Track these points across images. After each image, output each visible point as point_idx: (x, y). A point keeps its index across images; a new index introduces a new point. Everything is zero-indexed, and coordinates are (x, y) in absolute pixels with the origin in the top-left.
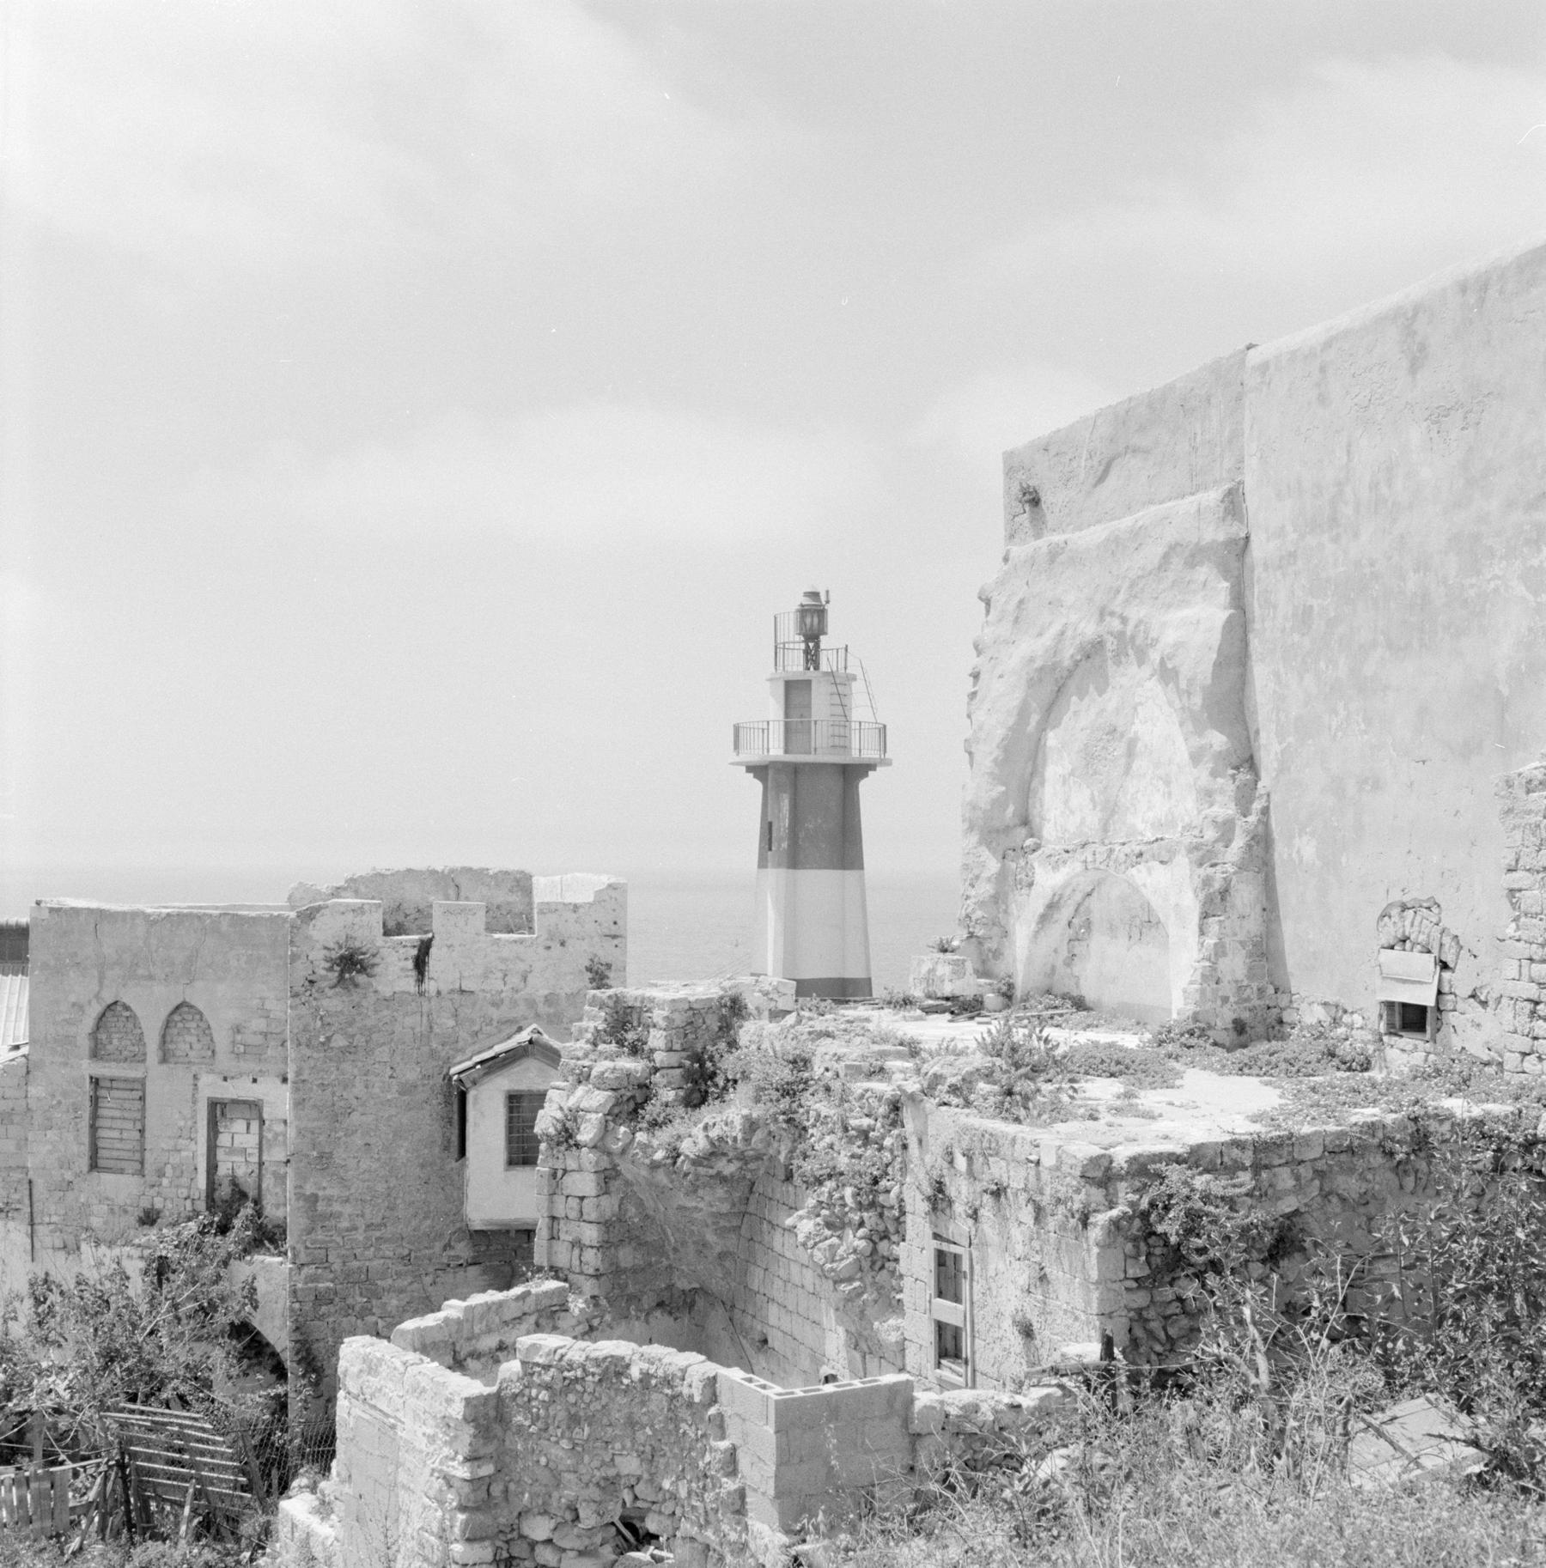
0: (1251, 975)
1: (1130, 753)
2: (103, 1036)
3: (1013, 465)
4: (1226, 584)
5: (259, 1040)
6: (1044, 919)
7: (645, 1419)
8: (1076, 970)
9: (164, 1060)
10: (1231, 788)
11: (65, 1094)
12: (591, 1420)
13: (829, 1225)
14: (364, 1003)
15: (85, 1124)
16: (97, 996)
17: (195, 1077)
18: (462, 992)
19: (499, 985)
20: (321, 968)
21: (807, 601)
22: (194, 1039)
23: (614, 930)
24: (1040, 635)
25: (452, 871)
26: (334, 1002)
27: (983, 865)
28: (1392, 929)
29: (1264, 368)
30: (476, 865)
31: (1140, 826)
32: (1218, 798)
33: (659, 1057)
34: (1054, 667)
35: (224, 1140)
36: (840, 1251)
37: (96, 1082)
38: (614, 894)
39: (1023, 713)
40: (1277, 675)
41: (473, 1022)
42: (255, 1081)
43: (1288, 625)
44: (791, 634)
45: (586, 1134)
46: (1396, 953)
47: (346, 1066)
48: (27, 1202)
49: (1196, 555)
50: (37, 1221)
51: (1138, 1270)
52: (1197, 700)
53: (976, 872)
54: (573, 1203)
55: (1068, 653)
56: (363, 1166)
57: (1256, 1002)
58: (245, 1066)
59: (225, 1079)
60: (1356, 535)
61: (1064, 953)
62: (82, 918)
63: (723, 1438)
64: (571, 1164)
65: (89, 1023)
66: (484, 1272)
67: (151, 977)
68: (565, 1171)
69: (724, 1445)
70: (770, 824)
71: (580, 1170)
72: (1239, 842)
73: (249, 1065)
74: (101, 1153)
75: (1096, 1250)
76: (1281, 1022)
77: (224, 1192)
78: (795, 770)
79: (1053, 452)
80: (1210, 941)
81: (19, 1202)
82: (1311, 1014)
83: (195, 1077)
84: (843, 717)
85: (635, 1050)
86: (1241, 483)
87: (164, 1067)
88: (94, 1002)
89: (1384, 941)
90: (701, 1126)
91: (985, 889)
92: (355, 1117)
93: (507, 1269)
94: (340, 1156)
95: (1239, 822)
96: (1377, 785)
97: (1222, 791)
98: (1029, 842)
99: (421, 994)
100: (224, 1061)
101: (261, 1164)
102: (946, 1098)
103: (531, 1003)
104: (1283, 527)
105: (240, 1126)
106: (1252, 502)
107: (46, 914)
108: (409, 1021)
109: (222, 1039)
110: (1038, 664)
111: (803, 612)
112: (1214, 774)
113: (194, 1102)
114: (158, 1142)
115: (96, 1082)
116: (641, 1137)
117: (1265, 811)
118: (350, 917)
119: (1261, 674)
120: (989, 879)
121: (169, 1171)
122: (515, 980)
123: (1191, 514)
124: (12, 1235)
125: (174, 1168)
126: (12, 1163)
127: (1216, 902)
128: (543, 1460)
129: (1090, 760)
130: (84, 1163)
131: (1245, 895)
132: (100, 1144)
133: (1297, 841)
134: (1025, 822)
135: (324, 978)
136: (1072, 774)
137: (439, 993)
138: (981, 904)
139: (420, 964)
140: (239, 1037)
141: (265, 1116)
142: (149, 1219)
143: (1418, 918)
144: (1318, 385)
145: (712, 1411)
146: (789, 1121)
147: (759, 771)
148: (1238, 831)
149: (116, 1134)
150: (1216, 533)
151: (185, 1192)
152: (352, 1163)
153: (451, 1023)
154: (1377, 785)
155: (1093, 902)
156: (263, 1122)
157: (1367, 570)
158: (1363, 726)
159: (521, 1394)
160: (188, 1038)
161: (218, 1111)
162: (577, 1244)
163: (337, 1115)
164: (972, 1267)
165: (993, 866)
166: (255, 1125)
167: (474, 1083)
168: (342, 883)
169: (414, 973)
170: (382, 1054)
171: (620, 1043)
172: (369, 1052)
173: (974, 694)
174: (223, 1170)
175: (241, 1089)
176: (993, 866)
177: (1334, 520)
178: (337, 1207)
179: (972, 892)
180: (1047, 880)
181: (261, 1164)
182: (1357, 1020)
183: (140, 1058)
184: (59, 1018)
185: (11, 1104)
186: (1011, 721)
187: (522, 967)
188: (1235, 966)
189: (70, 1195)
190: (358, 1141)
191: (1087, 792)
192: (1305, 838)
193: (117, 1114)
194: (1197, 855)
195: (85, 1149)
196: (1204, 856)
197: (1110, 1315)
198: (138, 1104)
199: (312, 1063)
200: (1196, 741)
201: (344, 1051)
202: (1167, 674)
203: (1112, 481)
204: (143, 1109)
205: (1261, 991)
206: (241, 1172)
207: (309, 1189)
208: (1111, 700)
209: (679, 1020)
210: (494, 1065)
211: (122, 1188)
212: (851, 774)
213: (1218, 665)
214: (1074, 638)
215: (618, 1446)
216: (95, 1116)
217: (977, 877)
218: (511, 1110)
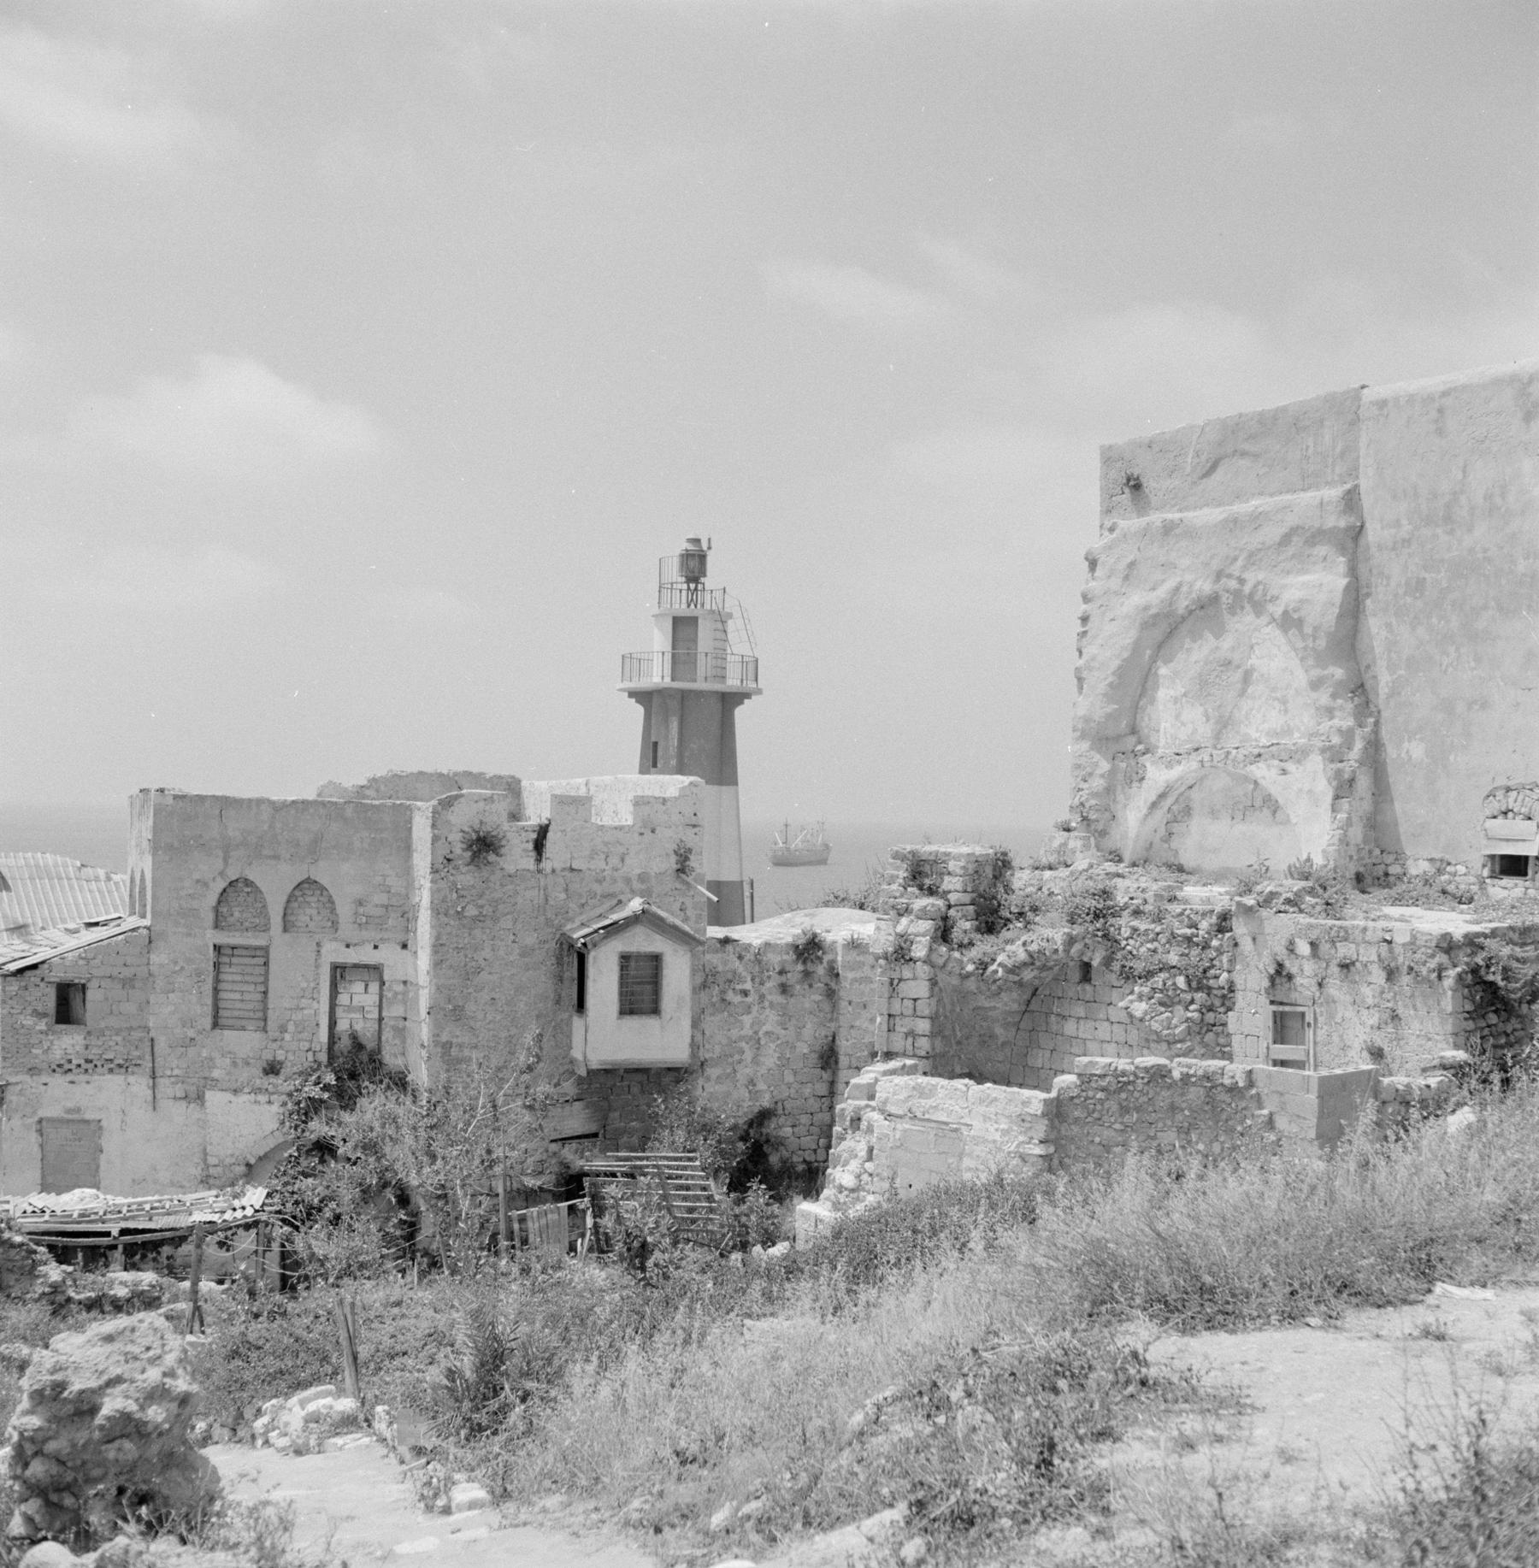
0: (1365, 842)
1: (1247, 678)
2: (224, 910)
3: (1109, 457)
4: (1342, 559)
5: (380, 912)
6: (1154, 805)
7: (1184, 1105)
8: (1174, 845)
9: (285, 930)
10: (1350, 706)
11: (189, 961)
12: (1138, 1109)
13: (1162, 1004)
14: (492, 878)
15: (208, 987)
16: (221, 874)
17: (318, 944)
18: (572, 870)
19: (602, 865)
20: (458, 849)
21: (691, 547)
22: (314, 912)
23: (694, 820)
24: (1154, 589)
25: (456, 774)
26: (467, 878)
27: (1096, 765)
28: (1496, 805)
29: (1382, 404)
30: (475, 770)
31: (1255, 735)
32: (1337, 713)
33: (953, 898)
34: (1168, 615)
35: (343, 999)
36: (1174, 1021)
37: (217, 948)
38: (694, 790)
39: (1137, 648)
40: (1389, 626)
41: (580, 896)
42: (376, 947)
43: (1401, 591)
44: (674, 574)
45: (919, 951)
46: (1500, 820)
47: (477, 932)
48: (148, 1057)
49: (1316, 537)
50: (159, 1073)
51: (1469, 1007)
52: (1322, 643)
53: (1089, 770)
54: (910, 1004)
55: (1182, 605)
56: (489, 1017)
57: (1368, 861)
58: (365, 934)
59: (348, 946)
60: (1470, 530)
61: (1162, 832)
62: (207, 804)
63: (1261, 1107)
64: (907, 974)
65: (212, 899)
66: (587, 1107)
67: (276, 857)
68: (900, 980)
69: (1265, 1112)
70: (655, 744)
71: (915, 978)
72: (1359, 745)
73: (371, 934)
74: (221, 1012)
75: (1450, 993)
76: (1387, 874)
77: (344, 1044)
78: (685, 698)
79: (1156, 448)
80: (1342, 816)
81: (139, 1058)
82: (1418, 867)
83: (318, 944)
84: (720, 656)
85: (931, 892)
86: (1357, 486)
87: (287, 936)
88: (219, 879)
89: (1488, 813)
90: (1020, 942)
91: (1098, 783)
92: (484, 975)
93: (605, 1104)
94: (471, 1008)
95: (1358, 731)
96: (1485, 705)
97: (1341, 708)
98: (1140, 747)
99: (539, 871)
100: (347, 930)
101: (381, 1019)
102: (1283, 908)
103: (628, 881)
104: (1398, 521)
105: (358, 987)
106: (1367, 502)
107: (170, 801)
108: (529, 894)
109: (344, 910)
110: (1153, 611)
111: (686, 557)
112: (1334, 696)
113: (317, 967)
114: (279, 1002)
115: (217, 948)
116: (956, 954)
117: (1377, 724)
118: (481, 804)
119: (1375, 626)
120: (1102, 776)
121: (291, 1027)
122: (614, 861)
123: (1317, 502)
124: (134, 1089)
125: (296, 1025)
126: (135, 1024)
127: (1344, 788)
128: (1097, 1140)
129: (1203, 687)
130: (207, 1022)
131: (1364, 783)
132: (222, 1004)
133: (1406, 744)
134: (1134, 731)
135: (460, 857)
136: (1185, 695)
137: (553, 871)
138: (1094, 795)
139: (539, 846)
140: (361, 910)
141: (386, 978)
142: (272, 1069)
143: (1521, 797)
144: (1436, 421)
145: (1254, 1091)
146: (1104, 936)
147: (643, 697)
148: (1357, 738)
149: (237, 996)
150: (1337, 521)
151: (307, 1045)
152: (480, 1015)
153: (563, 896)
154: (1485, 705)
155: (1195, 795)
156: (383, 983)
157: (1480, 556)
158: (1473, 664)
159: (1078, 1096)
160: (308, 911)
161: (339, 973)
162: (911, 1034)
163: (469, 974)
164: (1316, 1019)
165: (1105, 766)
166: (374, 987)
167: (595, 945)
168: (364, 782)
169: (533, 854)
170: (506, 923)
171: (921, 888)
172: (496, 920)
173: (1085, 633)
174: (343, 1026)
175: (366, 955)
176: (1105, 766)
177: (1448, 519)
178: (466, 1053)
179: (1085, 786)
180: (1158, 776)
181: (381, 1019)
182: (1461, 869)
183: (266, 928)
184: (183, 893)
185: (132, 970)
186: (1126, 655)
187: (621, 850)
188: (1357, 833)
189: (192, 1051)
190: (485, 996)
191: (1201, 709)
192: (1414, 743)
193: (239, 978)
194: (1328, 754)
195: (209, 1009)
196: (1334, 755)
197: (1456, 1034)
198: (262, 970)
199: (449, 929)
200: (1316, 673)
201: (475, 919)
202: (1289, 622)
203: (1218, 475)
204: (267, 972)
205: (1370, 852)
206: (358, 1027)
207: (444, 1038)
208: (1227, 643)
209: (971, 868)
210: (613, 929)
211: (246, 1042)
212: (729, 701)
213: (1340, 616)
214: (1190, 593)
215: (1160, 1125)
216: (217, 981)
217: (1091, 774)
218: (622, 968)
